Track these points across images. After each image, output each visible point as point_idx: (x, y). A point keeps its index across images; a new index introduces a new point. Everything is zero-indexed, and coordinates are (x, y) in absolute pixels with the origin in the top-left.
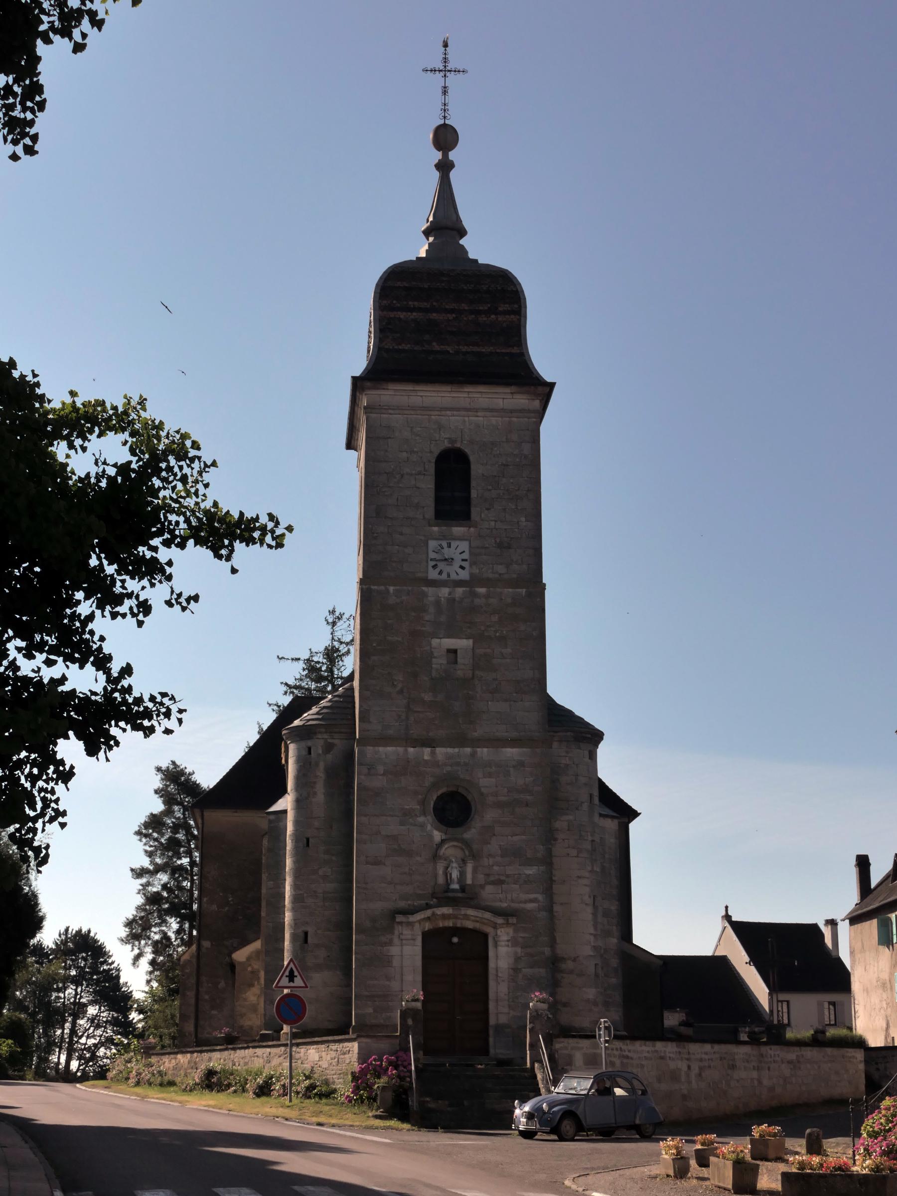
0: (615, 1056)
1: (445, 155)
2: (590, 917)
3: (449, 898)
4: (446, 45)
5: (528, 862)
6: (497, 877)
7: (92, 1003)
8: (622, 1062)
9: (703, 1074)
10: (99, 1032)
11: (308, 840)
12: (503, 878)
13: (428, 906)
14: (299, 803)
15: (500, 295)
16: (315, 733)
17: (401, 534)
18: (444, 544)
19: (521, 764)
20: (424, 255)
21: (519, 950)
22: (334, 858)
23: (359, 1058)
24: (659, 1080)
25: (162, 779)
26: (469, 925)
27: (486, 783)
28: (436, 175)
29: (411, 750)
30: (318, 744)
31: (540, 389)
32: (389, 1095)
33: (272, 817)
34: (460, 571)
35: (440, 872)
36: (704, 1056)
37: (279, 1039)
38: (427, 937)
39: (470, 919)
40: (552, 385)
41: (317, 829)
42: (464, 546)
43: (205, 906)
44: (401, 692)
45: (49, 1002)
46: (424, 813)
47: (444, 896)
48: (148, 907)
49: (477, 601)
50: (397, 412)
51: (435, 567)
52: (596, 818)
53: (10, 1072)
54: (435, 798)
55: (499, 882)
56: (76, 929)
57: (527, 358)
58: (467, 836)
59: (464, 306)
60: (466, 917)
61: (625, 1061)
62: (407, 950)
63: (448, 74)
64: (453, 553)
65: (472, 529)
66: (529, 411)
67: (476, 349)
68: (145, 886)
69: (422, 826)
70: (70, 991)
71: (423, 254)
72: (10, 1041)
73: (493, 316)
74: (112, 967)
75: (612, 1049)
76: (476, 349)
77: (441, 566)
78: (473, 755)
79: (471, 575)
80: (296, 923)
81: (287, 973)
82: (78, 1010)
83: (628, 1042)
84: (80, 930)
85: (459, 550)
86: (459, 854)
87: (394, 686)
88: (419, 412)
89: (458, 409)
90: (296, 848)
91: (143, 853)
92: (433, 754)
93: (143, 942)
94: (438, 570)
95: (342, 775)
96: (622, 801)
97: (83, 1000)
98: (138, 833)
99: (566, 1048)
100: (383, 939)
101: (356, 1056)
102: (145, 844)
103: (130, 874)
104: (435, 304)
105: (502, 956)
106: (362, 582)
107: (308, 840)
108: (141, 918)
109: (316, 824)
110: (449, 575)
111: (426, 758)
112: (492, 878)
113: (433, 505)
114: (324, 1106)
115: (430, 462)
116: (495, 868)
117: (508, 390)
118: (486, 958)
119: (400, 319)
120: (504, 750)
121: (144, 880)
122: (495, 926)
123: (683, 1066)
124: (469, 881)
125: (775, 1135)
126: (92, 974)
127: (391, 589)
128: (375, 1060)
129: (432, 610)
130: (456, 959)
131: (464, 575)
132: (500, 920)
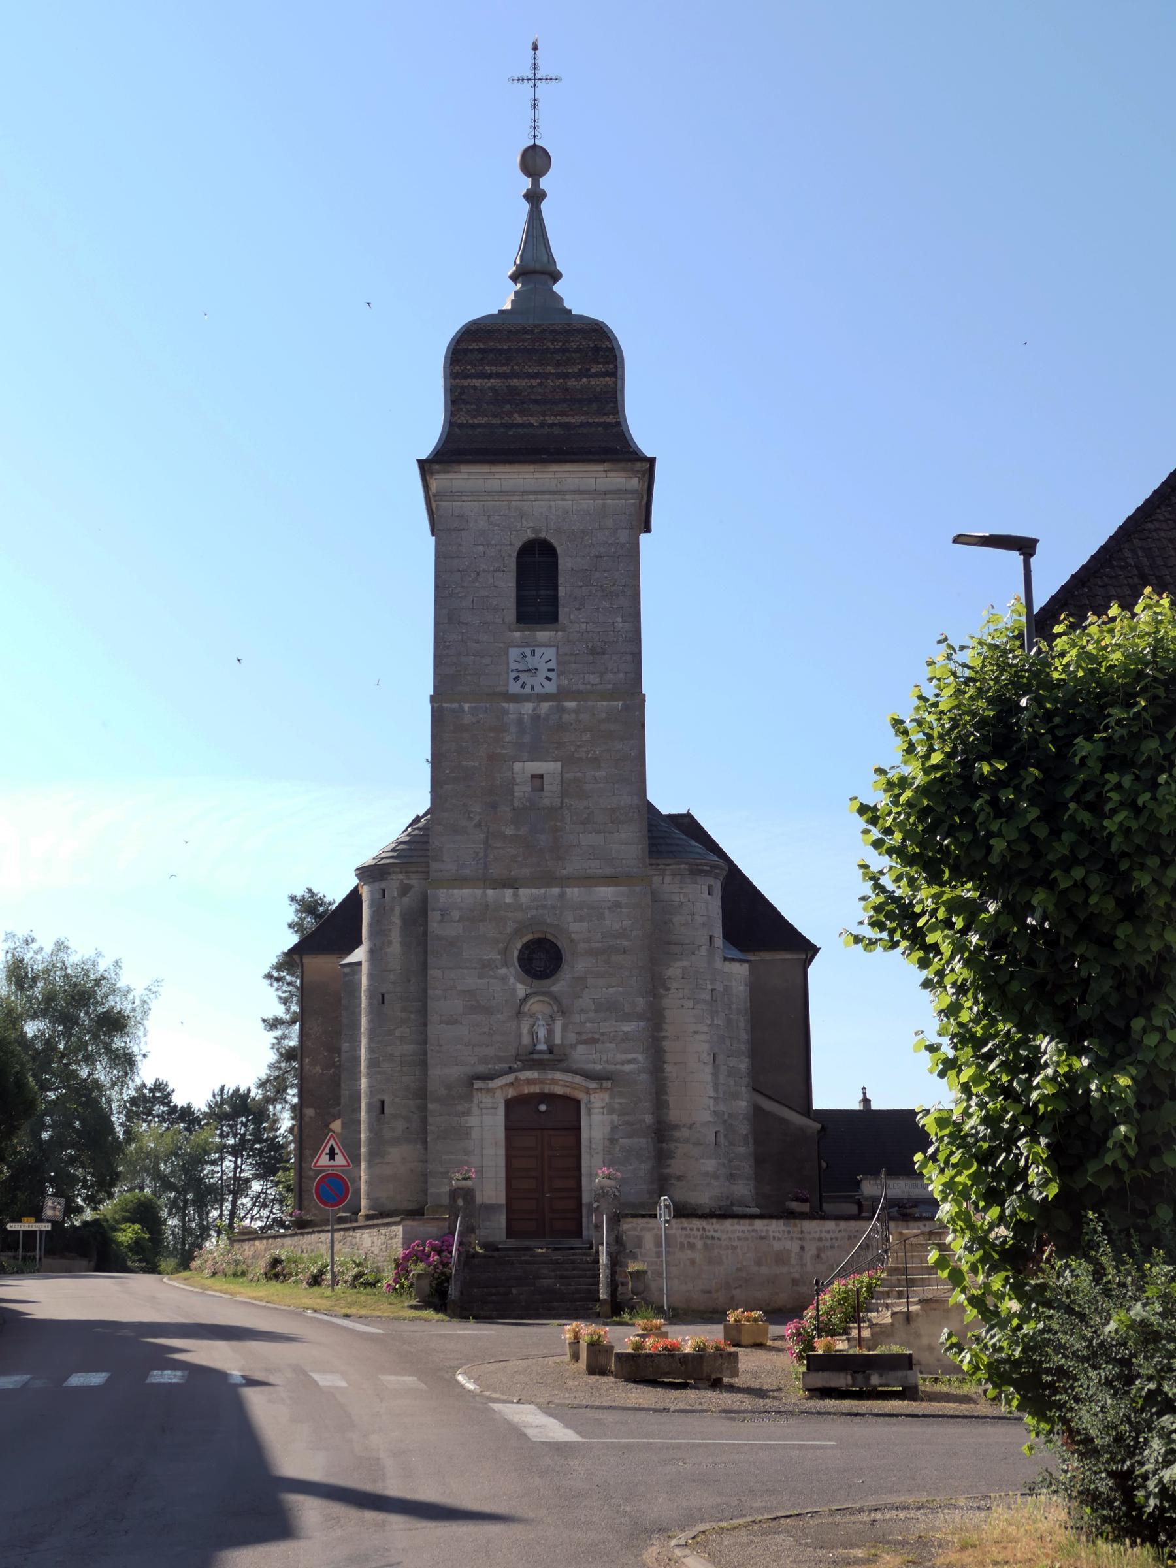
0: (695, 1237)
1: (536, 183)
2: (709, 1078)
3: (533, 1060)
4: (535, 48)
5: (627, 1017)
6: (590, 1035)
7: (256, 1177)
8: (705, 1244)
9: (823, 1256)
10: (265, 1212)
11: (383, 995)
12: (597, 1036)
13: (511, 1070)
14: (372, 952)
15: (596, 349)
16: (389, 874)
17: (477, 642)
18: (527, 651)
19: (617, 905)
20: (509, 307)
21: (615, 1117)
22: (412, 1016)
23: (404, 1244)
24: (759, 1263)
25: (297, 911)
26: (559, 1090)
27: (577, 928)
28: (525, 206)
29: (490, 892)
30: (392, 886)
31: (638, 465)
32: (425, 1285)
33: (347, 970)
34: (546, 683)
35: (525, 1031)
36: (823, 1235)
37: (356, 1221)
38: (509, 1104)
39: (559, 1083)
40: (652, 461)
41: (394, 983)
42: (550, 653)
43: (307, 1068)
44: (478, 825)
45: (200, 1180)
46: (506, 964)
47: (530, 1059)
48: (283, 1065)
49: (566, 718)
50: (471, 498)
51: (516, 679)
52: (719, 963)
53: (129, 1263)
54: (519, 946)
55: (592, 1041)
56: (233, 1087)
57: (623, 428)
58: (555, 989)
59: (550, 369)
60: (554, 1082)
61: (709, 1242)
62: (488, 1120)
63: (538, 83)
64: (540, 658)
65: (560, 633)
66: (626, 491)
67: (566, 420)
68: (279, 1040)
69: (504, 979)
70: (228, 1163)
71: (508, 306)
72: (137, 1226)
73: (585, 380)
74: (278, 1134)
75: (692, 1229)
76: (560, 419)
77: (524, 677)
78: (562, 896)
79: (558, 686)
80: (372, 1090)
81: (327, 1150)
82: (239, 1186)
83: (714, 1220)
84: (238, 1090)
85: (546, 658)
86: (547, 1010)
87: (470, 818)
88: (496, 498)
89: (543, 493)
90: (370, 1005)
91: (276, 1000)
92: (515, 895)
93: (279, 1107)
94: (520, 683)
95: (418, 919)
96: (800, 934)
97: (246, 1175)
98: (269, 976)
99: (635, 1229)
100: (459, 1108)
101: (401, 1240)
102: (277, 990)
103: (262, 1025)
104: (516, 367)
105: (596, 1125)
106: (433, 699)
107: (383, 995)
108: (276, 1078)
109: (392, 977)
110: (533, 688)
111: (508, 900)
112: (584, 1037)
113: (514, 606)
114: (364, 1295)
115: (510, 556)
116: (588, 1025)
117: (599, 467)
118: (579, 1128)
119: (475, 388)
120: (598, 889)
121: (278, 1033)
122: (588, 1091)
123: (795, 1247)
124: (558, 1041)
125: (755, 1320)
126: (255, 1142)
127: (466, 706)
128: (418, 1245)
129: (513, 729)
130: (544, 1131)
131: (551, 688)
132: (593, 1085)
